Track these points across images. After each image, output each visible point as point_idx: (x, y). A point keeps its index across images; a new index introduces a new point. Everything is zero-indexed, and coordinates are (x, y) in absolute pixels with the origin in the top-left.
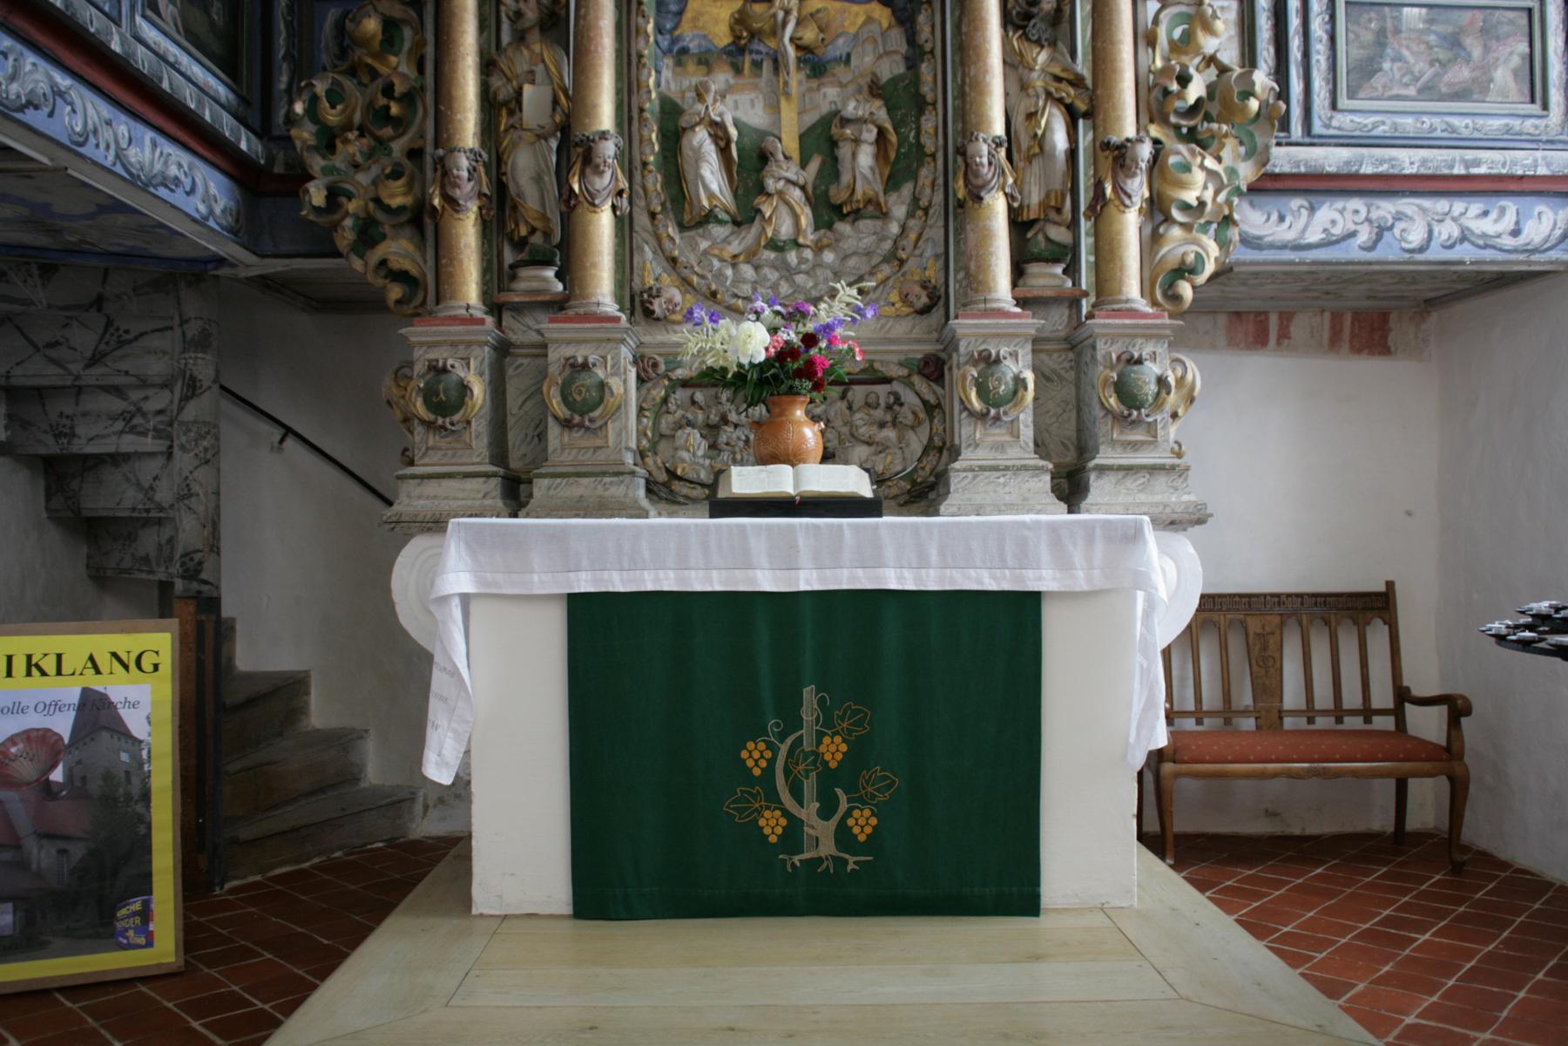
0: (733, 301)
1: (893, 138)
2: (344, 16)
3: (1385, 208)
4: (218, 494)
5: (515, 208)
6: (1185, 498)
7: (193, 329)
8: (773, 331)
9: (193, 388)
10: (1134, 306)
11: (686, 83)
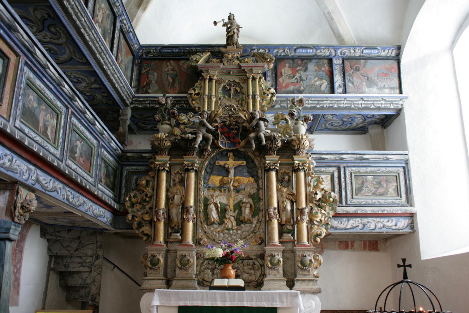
0: (218, 241)
1: (253, 206)
2: (138, 178)
3: (365, 220)
4: (101, 281)
5: (172, 221)
6: (316, 287)
7: (99, 244)
8: (224, 250)
9: (98, 257)
10: (305, 244)
11: (210, 194)
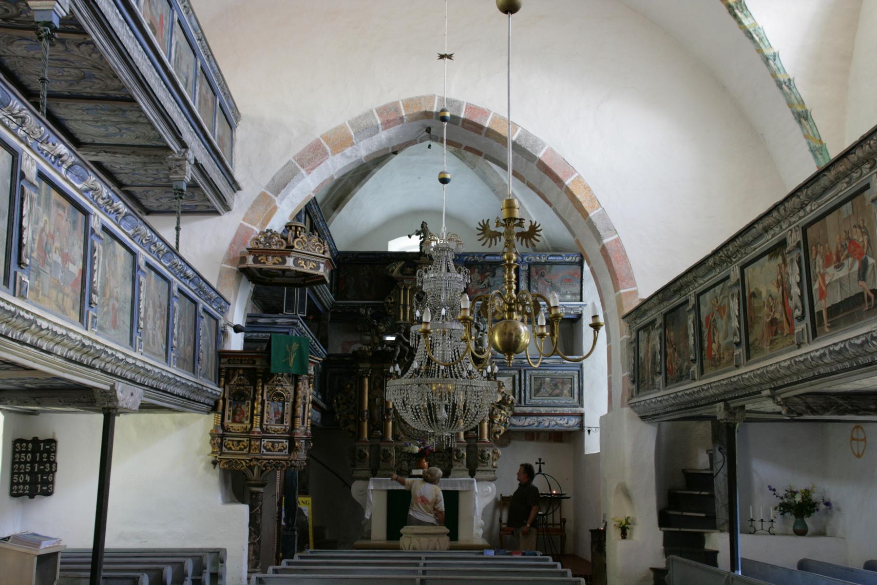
3: (541, 419)
